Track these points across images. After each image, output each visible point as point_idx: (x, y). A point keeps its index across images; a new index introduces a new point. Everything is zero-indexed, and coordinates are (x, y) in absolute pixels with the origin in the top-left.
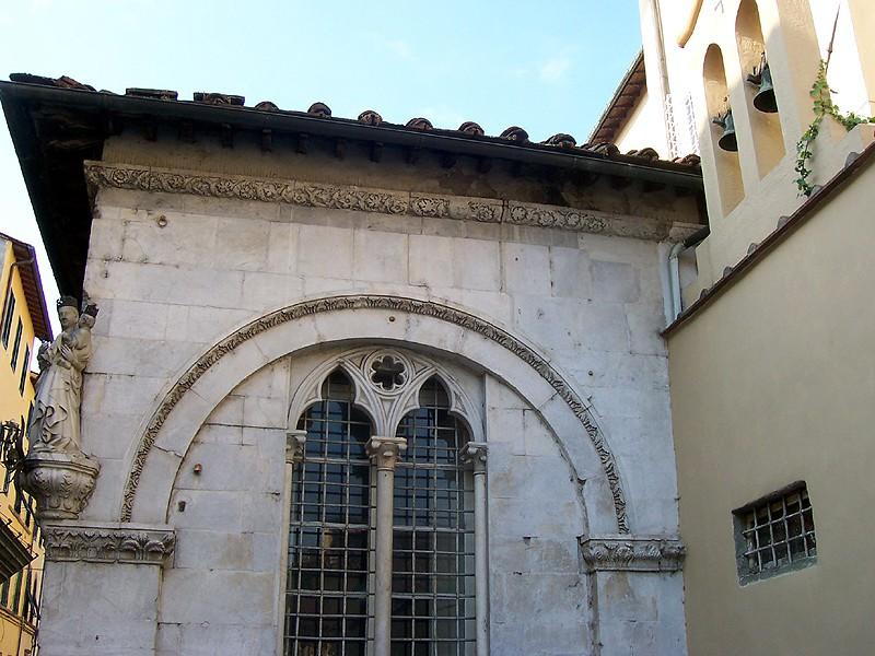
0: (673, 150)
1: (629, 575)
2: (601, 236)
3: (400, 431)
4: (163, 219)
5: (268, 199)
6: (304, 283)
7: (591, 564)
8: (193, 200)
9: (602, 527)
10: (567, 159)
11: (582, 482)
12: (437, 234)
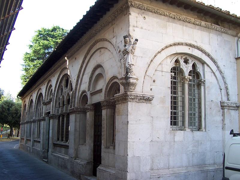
0: (159, 13)
2: (226, 34)
3: (189, 75)
5: (166, 16)
6: (174, 38)
7: (223, 107)
8: (150, 13)
9: (225, 99)
10: (228, 17)
11: (221, 89)
12: (198, 30)
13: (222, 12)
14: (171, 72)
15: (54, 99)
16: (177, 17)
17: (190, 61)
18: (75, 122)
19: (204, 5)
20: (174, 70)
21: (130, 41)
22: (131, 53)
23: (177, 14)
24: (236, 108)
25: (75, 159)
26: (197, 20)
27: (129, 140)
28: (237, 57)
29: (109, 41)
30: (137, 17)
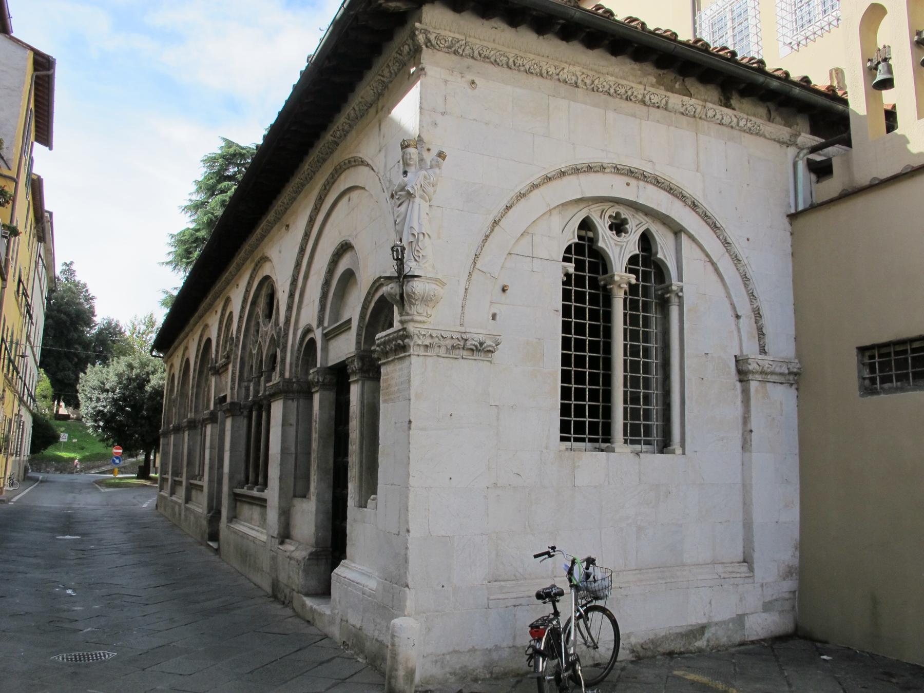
0: (522, 69)
1: (768, 385)
4: (473, 82)
7: (743, 374)
9: (751, 349)
11: (738, 317)
12: (658, 121)
13: (736, 62)
14: (565, 259)
15: (237, 355)
16: (586, 80)
17: (631, 225)
18: (283, 425)
19: (673, 38)
20: (575, 252)
21: (421, 160)
22: (422, 197)
23: (585, 71)
24: (787, 377)
25: (282, 543)
26: (652, 90)
27: (412, 481)
28: (793, 211)
29: (368, 165)
30: (446, 82)
